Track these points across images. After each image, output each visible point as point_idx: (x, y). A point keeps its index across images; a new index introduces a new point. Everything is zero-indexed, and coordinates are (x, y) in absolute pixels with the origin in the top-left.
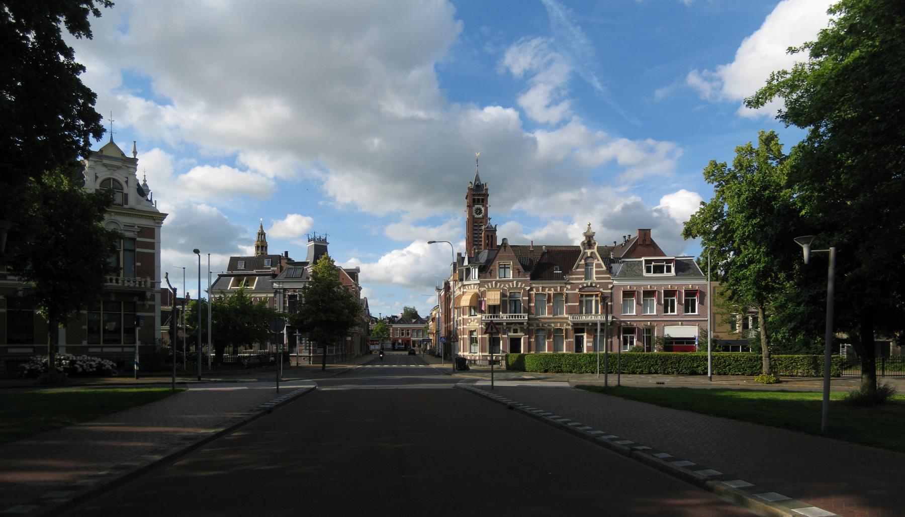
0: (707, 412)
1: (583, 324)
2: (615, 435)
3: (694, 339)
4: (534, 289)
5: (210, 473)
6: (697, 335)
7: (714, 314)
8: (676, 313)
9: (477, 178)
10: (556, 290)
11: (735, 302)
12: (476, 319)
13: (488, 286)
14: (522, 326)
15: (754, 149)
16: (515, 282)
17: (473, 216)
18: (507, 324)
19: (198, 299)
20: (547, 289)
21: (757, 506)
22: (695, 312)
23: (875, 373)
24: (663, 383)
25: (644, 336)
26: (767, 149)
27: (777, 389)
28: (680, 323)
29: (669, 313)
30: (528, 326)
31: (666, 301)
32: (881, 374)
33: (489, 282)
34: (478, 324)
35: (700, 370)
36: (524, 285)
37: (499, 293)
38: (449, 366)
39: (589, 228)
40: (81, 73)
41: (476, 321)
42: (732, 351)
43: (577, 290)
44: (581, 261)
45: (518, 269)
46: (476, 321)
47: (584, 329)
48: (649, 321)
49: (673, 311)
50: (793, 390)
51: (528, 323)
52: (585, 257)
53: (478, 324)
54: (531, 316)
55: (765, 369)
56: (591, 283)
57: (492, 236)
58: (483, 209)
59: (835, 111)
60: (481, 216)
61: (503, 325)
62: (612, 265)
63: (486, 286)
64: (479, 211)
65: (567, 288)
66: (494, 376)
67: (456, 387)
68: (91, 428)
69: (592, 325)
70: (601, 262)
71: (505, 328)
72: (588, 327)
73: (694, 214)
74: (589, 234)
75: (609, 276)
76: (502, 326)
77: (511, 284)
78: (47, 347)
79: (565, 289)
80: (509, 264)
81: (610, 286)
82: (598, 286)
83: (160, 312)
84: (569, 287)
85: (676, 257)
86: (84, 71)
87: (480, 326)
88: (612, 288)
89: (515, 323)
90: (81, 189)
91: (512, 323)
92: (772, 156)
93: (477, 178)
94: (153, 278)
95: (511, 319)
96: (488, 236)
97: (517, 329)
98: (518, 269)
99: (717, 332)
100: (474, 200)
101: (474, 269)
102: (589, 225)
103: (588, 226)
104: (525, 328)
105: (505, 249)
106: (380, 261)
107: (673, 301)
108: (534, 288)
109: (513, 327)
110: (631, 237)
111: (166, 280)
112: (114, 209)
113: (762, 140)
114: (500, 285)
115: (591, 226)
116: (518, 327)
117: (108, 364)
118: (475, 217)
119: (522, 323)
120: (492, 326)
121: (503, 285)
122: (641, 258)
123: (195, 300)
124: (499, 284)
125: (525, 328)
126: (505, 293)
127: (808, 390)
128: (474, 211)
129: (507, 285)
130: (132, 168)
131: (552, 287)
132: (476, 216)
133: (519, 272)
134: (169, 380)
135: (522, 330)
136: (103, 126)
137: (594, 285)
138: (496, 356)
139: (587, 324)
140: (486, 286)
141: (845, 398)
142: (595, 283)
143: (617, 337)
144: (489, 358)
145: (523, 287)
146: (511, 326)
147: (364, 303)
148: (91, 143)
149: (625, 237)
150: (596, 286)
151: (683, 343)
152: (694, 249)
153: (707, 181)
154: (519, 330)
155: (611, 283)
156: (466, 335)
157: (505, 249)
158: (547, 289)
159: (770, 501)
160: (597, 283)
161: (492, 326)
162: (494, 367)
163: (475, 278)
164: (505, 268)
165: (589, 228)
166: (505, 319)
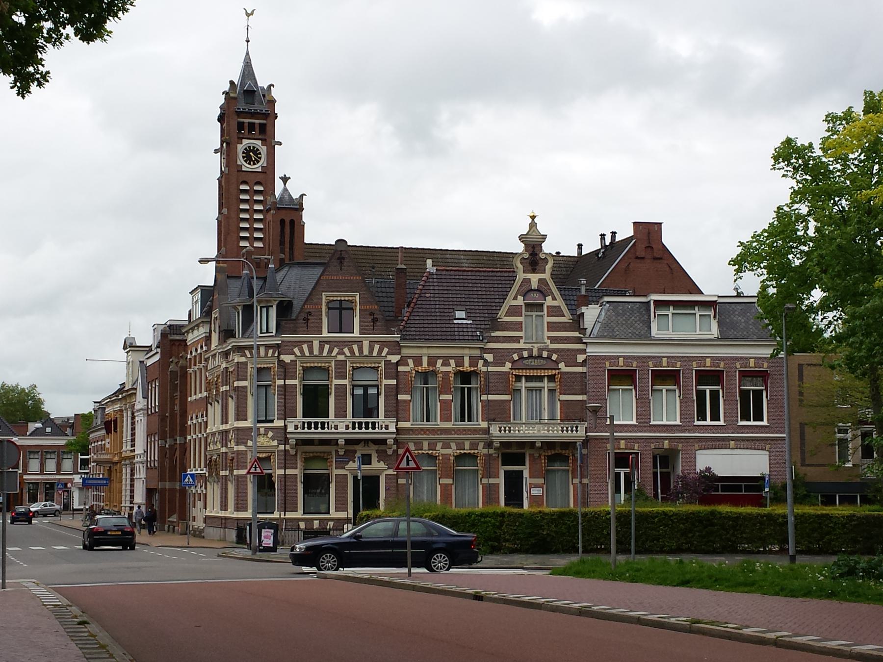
0: (310, 294)
1: (522, 445)
3: (762, 478)
4: (410, 361)
6: (766, 471)
7: (802, 425)
8: (765, 423)
9: (248, 70)
10: (460, 446)
12: (271, 429)
13: (302, 351)
14: (382, 447)
15: (43, 66)
16: (366, 344)
17: (264, 141)
18: (348, 442)
19: (215, 262)
20: (440, 362)
22: (762, 420)
23: (596, 253)
24: (219, 556)
25: (655, 474)
28: (732, 443)
29: (708, 422)
30: (395, 447)
31: (701, 395)
33: (304, 342)
34: (275, 443)
35: (47, 498)
36: (386, 350)
38: (108, 656)
39: (533, 225)
41: (270, 434)
43: (508, 365)
44: (515, 298)
45: (372, 314)
46: (270, 434)
47: (523, 456)
48: (665, 438)
49: (715, 417)
51: (395, 440)
52: (525, 288)
53: (275, 443)
54: (403, 424)
56: (540, 350)
57: (292, 222)
58: (263, 150)
60: (240, 148)
61: (337, 444)
62: (584, 309)
63: (296, 350)
64: (251, 155)
65: (486, 361)
67: (713, 513)
68: (475, 398)
69: (541, 448)
70: (559, 302)
71: (341, 452)
72: (532, 451)
73: (772, 221)
74: (533, 238)
75: (576, 334)
76: (335, 447)
77: (355, 347)
78: (719, 492)
79: (481, 362)
80: (351, 302)
81: (581, 358)
82: (554, 357)
83: (797, 365)
84: (489, 357)
86: (852, 107)
87: (282, 447)
88: (584, 363)
89: (366, 442)
90: (765, 267)
91: (357, 442)
93: (248, 70)
95: (306, 430)
96: (282, 222)
97: (370, 455)
98: (372, 314)
99: (808, 465)
100: (241, 126)
101: (264, 310)
102: (533, 217)
103: (530, 220)
104: (390, 452)
105: (341, 263)
106: (806, 438)
107: (715, 395)
108: (410, 357)
109: (360, 451)
110: (618, 238)
112: (527, 401)
114: (330, 351)
115: (536, 220)
116: (372, 450)
117: (832, 137)
118: (244, 169)
119: (383, 442)
120: (408, 457)
121: (336, 350)
122: (308, 548)
123: (290, 195)
124: (327, 347)
125: (390, 452)
126: (214, 308)
127: (688, 315)
128: (240, 155)
129: (346, 350)
131: (452, 358)
132: (246, 167)
133: (374, 320)
134: (156, 458)
135: (383, 456)
136: (17, 386)
137: (545, 354)
138: (320, 520)
139: (532, 444)
140: (296, 350)
142: (548, 350)
144: (302, 525)
145: (334, 354)
146: (356, 447)
147: (770, 502)
148: (217, 181)
149: (603, 236)
150: (549, 358)
151: (739, 488)
153: (820, 146)
154: (374, 459)
155: (584, 351)
156: (279, 386)
157: (341, 263)
158: (440, 362)
160: (552, 351)
161: (408, 457)
162: (376, 390)
163: (267, 332)
164: (341, 309)
165: (533, 225)
166: (344, 430)
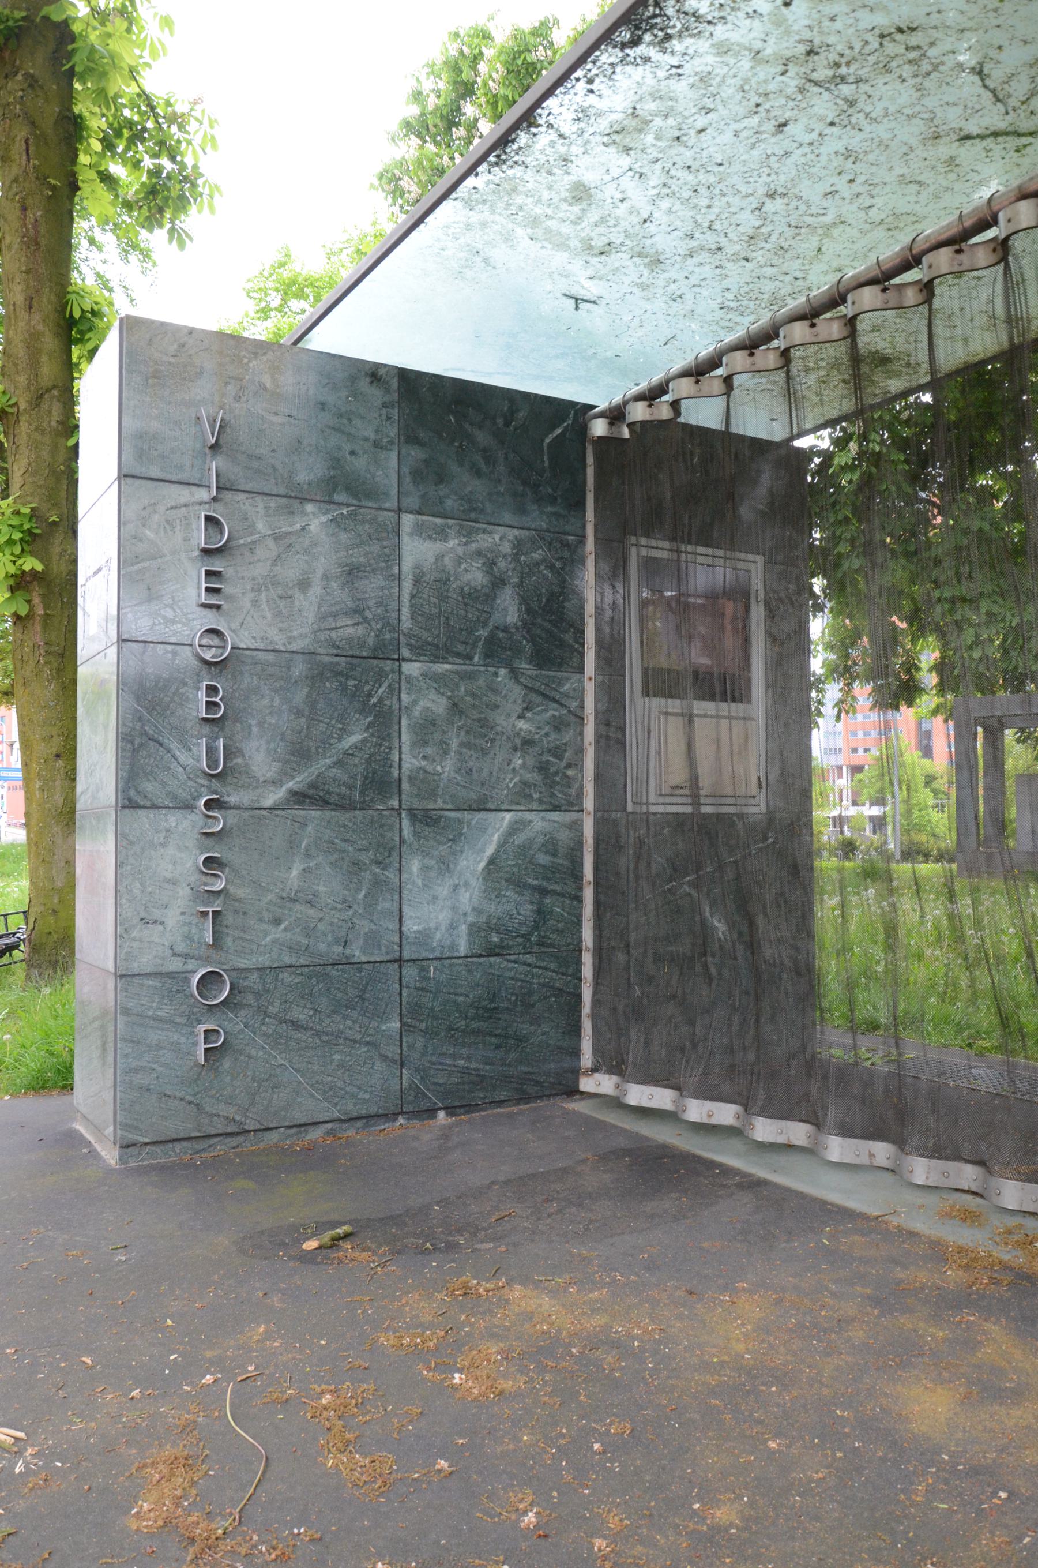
2: (975, 739)
5: (590, 472)
11: (871, 861)
21: (11, 716)
24: (759, 778)
26: (682, 203)
27: (732, 412)
32: (683, 555)
37: (695, 702)
40: (822, 668)
42: (207, 702)
50: (181, 486)
55: (929, 679)
59: (204, 1377)
66: (404, 972)
85: (810, 1151)
92: (367, 1096)
94: (983, 362)
111: (966, 1188)
113: (234, 676)
130: (538, 103)
141: (749, 336)
143: (944, 717)
152: (1010, 546)
159: (547, 441)
